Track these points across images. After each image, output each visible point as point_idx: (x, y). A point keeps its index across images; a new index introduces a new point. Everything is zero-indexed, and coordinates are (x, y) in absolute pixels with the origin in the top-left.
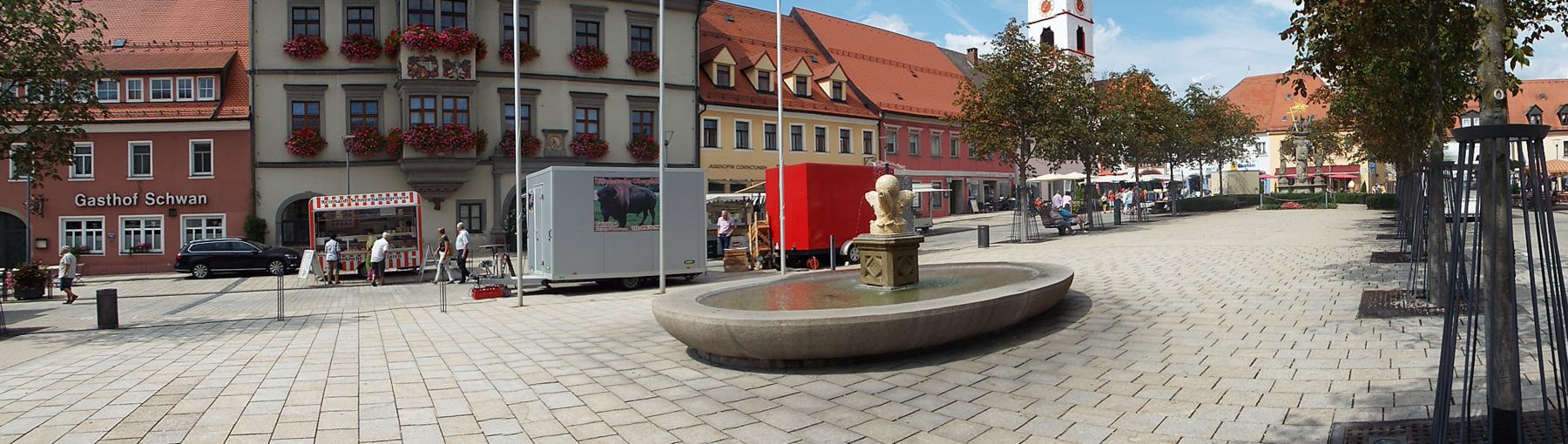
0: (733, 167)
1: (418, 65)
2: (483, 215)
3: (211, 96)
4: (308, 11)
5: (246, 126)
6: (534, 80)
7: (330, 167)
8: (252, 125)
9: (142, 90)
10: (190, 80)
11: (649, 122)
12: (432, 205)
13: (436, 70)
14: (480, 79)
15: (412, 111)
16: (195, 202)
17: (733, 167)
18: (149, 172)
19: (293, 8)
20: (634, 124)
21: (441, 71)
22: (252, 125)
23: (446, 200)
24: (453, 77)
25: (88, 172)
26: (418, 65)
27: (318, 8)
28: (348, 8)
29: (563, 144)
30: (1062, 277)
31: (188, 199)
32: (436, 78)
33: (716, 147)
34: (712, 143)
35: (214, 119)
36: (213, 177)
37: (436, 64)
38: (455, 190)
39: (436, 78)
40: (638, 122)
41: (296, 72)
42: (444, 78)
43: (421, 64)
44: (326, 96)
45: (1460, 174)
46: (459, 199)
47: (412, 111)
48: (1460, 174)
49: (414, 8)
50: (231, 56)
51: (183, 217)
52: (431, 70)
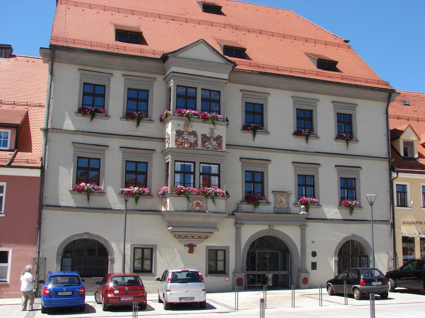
0: (421, 223)
3: (6, 146)
5: (37, 173)
7: (305, 236)
11: (259, 180)
12: (187, 249)
14: (229, 150)
17: (421, 223)
18: (416, 269)
20: (246, 182)
21: (200, 142)
24: (208, 148)
29: (288, 202)
30: (129, 256)
32: (196, 148)
33: (406, 207)
34: (403, 203)
35: (9, 166)
37: (197, 137)
38: (207, 237)
39: (196, 148)
40: (250, 179)
41: (83, 133)
42: (202, 148)
49: (99, 99)
50: (24, 114)
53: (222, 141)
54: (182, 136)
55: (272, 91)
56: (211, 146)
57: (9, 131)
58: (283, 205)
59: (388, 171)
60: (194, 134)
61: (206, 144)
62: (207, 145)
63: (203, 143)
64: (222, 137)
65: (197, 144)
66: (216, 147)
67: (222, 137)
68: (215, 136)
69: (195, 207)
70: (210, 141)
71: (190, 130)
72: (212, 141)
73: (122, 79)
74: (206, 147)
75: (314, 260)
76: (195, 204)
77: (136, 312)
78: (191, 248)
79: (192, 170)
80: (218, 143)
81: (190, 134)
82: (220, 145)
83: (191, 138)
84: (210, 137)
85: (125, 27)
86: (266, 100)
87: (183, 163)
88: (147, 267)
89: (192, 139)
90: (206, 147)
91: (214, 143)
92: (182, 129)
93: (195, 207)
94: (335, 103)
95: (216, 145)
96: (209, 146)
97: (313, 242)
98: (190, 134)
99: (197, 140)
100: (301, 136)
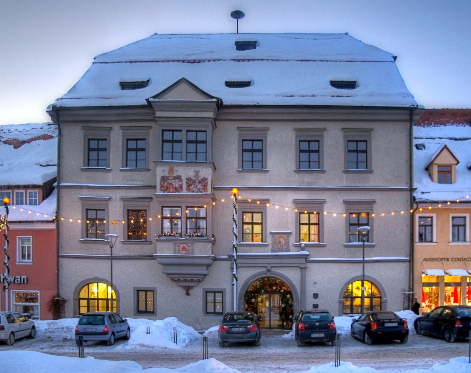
0: (448, 260)
1: (168, 183)
2: (205, 304)
4: (100, 141)
5: (53, 226)
6: (265, 192)
8: (58, 226)
9: (24, 199)
10: (23, 193)
12: (184, 291)
13: (181, 187)
15: (205, 218)
16: (19, 282)
19: (243, 140)
21: (185, 186)
22: (58, 226)
23: (194, 288)
25: (29, 258)
26: (168, 183)
27: (261, 140)
28: (300, 141)
31: (15, 279)
36: (31, 264)
37: (181, 181)
43: (170, 182)
44: (374, 208)
45: (362, 302)
46: (203, 287)
47: (205, 218)
48: (362, 302)
51: (13, 292)
52: (177, 186)
53: (207, 183)
54: (167, 182)
55: (272, 126)
56: (196, 189)
57: (37, 191)
58: (281, 246)
59: (409, 203)
60: (179, 178)
61: (191, 187)
62: (192, 188)
63: (189, 186)
64: (207, 179)
65: (182, 189)
66: (201, 190)
67: (207, 179)
68: (200, 179)
69: (182, 251)
70: (194, 184)
71: (175, 175)
72: (197, 184)
73: (121, 132)
74: (191, 190)
75: (315, 301)
76: (181, 248)
77: (279, 306)
78: (188, 290)
79: (203, 214)
80: (203, 185)
81: (175, 178)
82: (205, 187)
83: (175, 182)
84: (195, 180)
85: (193, 89)
86: (322, 136)
87: (171, 209)
88: (150, 308)
89: (176, 184)
90: (191, 190)
91: (200, 186)
92: (166, 174)
93: (182, 251)
94: (345, 130)
95: (201, 187)
96: (194, 189)
97: (315, 283)
98: (175, 178)
99: (182, 184)
100: (425, 168)
